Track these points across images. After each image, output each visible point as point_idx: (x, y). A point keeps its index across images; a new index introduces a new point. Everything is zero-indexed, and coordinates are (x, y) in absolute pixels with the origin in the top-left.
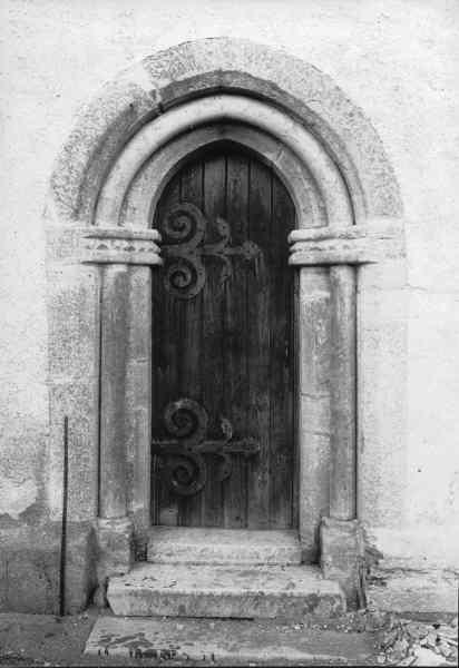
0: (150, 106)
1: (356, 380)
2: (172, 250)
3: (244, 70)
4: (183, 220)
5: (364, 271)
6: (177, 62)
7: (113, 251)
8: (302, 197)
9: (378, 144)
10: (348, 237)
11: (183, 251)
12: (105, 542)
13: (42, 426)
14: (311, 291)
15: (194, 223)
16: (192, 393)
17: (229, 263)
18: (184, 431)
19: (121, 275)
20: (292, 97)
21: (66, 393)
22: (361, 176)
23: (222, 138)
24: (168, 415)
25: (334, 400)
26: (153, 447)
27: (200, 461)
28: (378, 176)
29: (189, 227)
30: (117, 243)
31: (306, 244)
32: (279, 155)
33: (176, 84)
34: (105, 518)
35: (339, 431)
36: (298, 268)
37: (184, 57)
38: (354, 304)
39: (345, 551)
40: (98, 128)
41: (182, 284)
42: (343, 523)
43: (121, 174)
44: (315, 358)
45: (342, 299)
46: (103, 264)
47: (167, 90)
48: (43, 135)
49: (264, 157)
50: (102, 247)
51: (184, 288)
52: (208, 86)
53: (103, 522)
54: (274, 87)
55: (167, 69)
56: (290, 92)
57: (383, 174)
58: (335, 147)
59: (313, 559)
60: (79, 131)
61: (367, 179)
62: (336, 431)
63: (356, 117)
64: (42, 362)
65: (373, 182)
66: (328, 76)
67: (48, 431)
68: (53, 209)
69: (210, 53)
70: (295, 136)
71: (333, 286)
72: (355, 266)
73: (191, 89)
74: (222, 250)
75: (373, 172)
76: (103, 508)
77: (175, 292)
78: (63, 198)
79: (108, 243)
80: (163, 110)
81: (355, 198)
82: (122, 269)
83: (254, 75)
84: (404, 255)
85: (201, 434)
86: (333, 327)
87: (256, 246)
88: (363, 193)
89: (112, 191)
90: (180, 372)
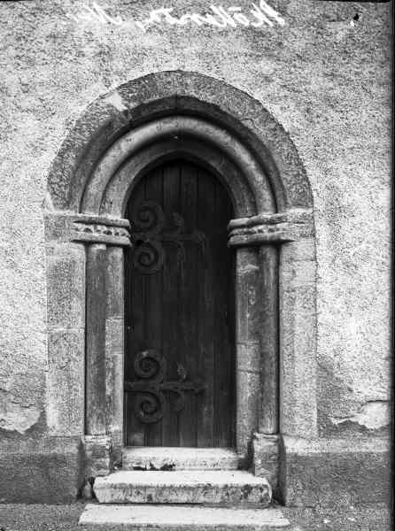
5: (286, 252)
14: (245, 266)
15: (156, 218)
18: (149, 374)
19: (101, 251)
22: (283, 176)
25: (261, 345)
27: (162, 397)
28: (295, 176)
29: (152, 219)
30: (99, 227)
34: (91, 435)
35: (267, 369)
44: (248, 315)
46: (88, 244)
47: (137, 110)
52: (168, 108)
53: (89, 438)
54: (217, 108)
56: (229, 113)
57: (298, 174)
69: (169, 83)
71: (260, 260)
75: (291, 173)
79: (91, 227)
81: (278, 193)
85: (162, 376)
89: (95, 189)
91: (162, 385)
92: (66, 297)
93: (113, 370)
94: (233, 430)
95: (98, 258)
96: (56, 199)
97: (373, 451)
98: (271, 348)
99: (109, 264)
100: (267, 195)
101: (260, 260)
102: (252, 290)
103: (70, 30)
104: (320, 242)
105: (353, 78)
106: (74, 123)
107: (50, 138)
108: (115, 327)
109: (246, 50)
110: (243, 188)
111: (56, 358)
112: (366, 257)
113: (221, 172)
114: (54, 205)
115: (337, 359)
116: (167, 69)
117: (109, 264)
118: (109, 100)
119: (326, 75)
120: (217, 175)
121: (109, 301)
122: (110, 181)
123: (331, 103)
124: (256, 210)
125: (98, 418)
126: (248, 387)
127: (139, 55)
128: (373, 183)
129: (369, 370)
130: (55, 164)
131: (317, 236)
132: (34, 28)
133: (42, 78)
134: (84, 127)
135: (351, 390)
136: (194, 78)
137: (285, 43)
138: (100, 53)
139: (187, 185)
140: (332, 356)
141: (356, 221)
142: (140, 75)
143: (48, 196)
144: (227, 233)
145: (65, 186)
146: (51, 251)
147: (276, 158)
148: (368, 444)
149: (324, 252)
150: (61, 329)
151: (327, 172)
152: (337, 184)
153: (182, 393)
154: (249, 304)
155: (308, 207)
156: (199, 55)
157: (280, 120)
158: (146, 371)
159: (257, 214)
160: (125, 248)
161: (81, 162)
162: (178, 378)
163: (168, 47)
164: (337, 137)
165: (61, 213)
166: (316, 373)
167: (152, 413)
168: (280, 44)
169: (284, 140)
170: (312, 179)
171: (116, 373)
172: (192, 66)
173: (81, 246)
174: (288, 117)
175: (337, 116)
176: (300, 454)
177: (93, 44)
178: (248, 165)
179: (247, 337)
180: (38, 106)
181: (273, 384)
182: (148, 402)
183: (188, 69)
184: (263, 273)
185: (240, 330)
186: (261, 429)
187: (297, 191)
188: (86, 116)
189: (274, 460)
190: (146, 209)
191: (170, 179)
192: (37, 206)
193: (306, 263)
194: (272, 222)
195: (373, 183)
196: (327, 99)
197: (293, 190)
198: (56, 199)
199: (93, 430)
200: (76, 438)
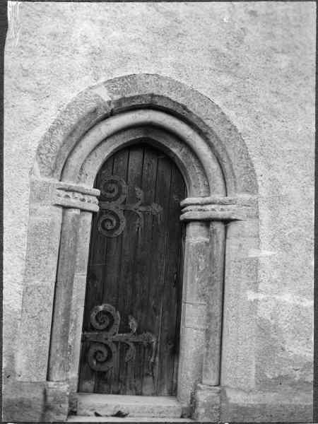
0: (106, 110)
1: (223, 293)
2: (106, 205)
3: (166, 94)
4: (114, 186)
5: (233, 228)
6: (126, 86)
7: (74, 200)
8: (193, 178)
9: (245, 149)
10: (222, 203)
11: (112, 206)
12: (52, 398)
13: (16, 313)
14: (195, 236)
15: (120, 188)
16: (111, 300)
17: (141, 216)
18: (102, 327)
19: (76, 215)
20: (195, 115)
21: (36, 292)
22: (234, 167)
23: (145, 136)
24: (93, 315)
25: (209, 306)
26: (83, 336)
27: (114, 349)
28: (244, 168)
29: (116, 192)
30: (77, 195)
31: (195, 207)
32: (181, 150)
33: (124, 99)
34: (52, 381)
35: (213, 327)
36: (187, 222)
37: (131, 83)
38: (225, 246)
39: (213, 406)
40: (72, 120)
41: (110, 228)
42: (213, 387)
43: (82, 151)
44: (197, 279)
45: (217, 242)
46: (65, 208)
47: (119, 102)
48: (34, 120)
49: (171, 151)
50: (67, 196)
51: (111, 230)
52: (144, 102)
53: (51, 384)
54: (185, 108)
55: (119, 89)
56: (194, 112)
57: (248, 167)
58: (219, 148)
59: (189, 415)
60: (59, 120)
61: (238, 170)
62: (210, 326)
63: (233, 132)
64: (20, 268)
65: (241, 171)
66: (217, 106)
67: (20, 316)
68: (37, 169)
69: (148, 83)
70: (193, 139)
71: (211, 234)
72: (226, 222)
73: (133, 104)
74: (137, 207)
75: (241, 165)
76: (50, 375)
77: (105, 233)
78: (45, 162)
79: (70, 194)
80: (112, 114)
81: (228, 181)
82: (77, 212)
83: (173, 99)
84: (258, 217)
85: (115, 328)
86: (211, 258)
87: (160, 207)
88: (235, 177)
89: (75, 162)
90: (103, 284)
91: (114, 337)
92: (44, 254)
93: (76, 321)
94: (175, 381)
95: (73, 221)
96: (43, 167)
97: (301, 403)
98: (216, 310)
99: (81, 226)
100: (219, 181)
101: (211, 234)
102: (201, 258)
103: (67, 33)
104: (263, 223)
105: (292, 97)
106: (65, 106)
107: (42, 115)
108: (81, 278)
109: (210, 66)
110: (199, 173)
111: (29, 308)
112: (298, 237)
113: (181, 158)
114: (41, 172)
115: (273, 322)
116: (146, 72)
117: (81, 226)
118: (96, 91)
119: (272, 92)
120: (176, 161)
121: (78, 260)
122: (88, 157)
123: (275, 114)
124: (209, 192)
125: (61, 365)
126: (194, 342)
127: (125, 59)
128: (305, 179)
129: (298, 333)
130: (45, 138)
131: (260, 218)
132: (38, 27)
133: (40, 66)
134: (74, 110)
135: (283, 349)
136: (168, 82)
137: (241, 64)
138: (92, 53)
139: (149, 165)
140: (269, 319)
141: (292, 208)
142: (124, 74)
143: (36, 165)
144: (180, 210)
145: (52, 159)
146: (32, 212)
147: (230, 152)
148: (296, 398)
149: (265, 231)
150: (37, 282)
151: (270, 167)
152: (278, 177)
153: (131, 345)
154: (198, 269)
155: (253, 193)
156: (174, 65)
157: (235, 123)
158: (101, 324)
159: (209, 196)
160: (94, 213)
161: (67, 138)
162: (129, 331)
163: (148, 56)
164: (279, 140)
165: (47, 180)
166: (256, 333)
167: (102, 363)
168: (237, 64)
169: (238, 139)
170: (258, 172)
171: (77, 325)
172: (167, 72)
173: (60, 210)
174: (241, 122)
175: (279, 124)
176: (240, 405)
177: (87, 45)
178: (206, 155)
179: (195, 298)
180: (35, 89)
181: (217, 340)
182: (101, 352)
183: (163, 74)
184: (213, 243)
185: (188, 292)
186: (204, 381)
187: (245, 181)
188: (75, 102)
189: (216, 409)
190: (112, 182)
191: (135, 159)
192: (26, 172)
193: (250, 239)
194: (222, 203)
195: (305, 179)
196: (272, 111)
197: (243, 179)
198: (43, 167)
199: (56, 376)
200: (41, 384)
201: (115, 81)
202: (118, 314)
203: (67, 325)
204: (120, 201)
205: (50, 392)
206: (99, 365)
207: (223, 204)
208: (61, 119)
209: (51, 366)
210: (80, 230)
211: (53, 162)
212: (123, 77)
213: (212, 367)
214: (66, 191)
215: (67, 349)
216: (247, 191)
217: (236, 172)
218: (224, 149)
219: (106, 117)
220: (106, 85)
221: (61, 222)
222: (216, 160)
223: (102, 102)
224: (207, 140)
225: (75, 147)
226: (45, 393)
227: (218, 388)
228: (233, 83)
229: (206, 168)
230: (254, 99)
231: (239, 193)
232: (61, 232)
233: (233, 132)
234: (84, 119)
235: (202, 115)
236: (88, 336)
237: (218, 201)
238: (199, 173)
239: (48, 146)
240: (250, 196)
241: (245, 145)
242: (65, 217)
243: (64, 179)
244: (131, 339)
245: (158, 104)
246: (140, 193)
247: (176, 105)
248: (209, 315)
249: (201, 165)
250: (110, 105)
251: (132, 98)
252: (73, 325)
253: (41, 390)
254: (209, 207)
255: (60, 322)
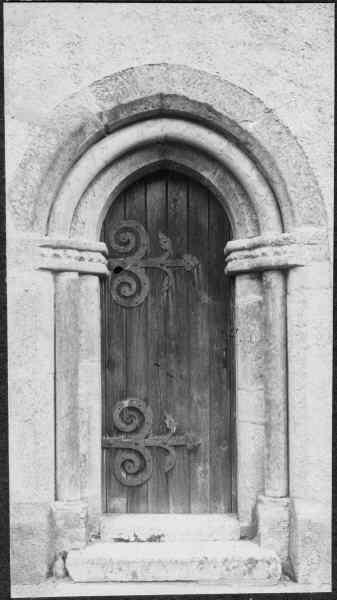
4: (129, 236)
5: (293, 275)
7: (67, 260)
10: (278, 244)
14: (245, 294)
15: (138, 242)
17: (171, 274)
18: (131, 428)
19: (72, 281)
23: (162, 158)
25: (267, 391)
27: (147, 454)
29: (133, 241)
30: (69, 252)
31: (240, 253)
32: (214, 173)
33: (121, 107)
36: (233, 276)
38: (285, 305)
39: (279, 524)
46: (56, 272)
47: (114, 112)
50: (56, 256)
52: (151, 109)
54: (210, 109)
56: (225, 113)
66: (259, 99)
71: (265, 289)
72: (284, 271)
73: (135, 112)
77: (121, 301)
78: (19, 211)
79: (60, 252)
80: (108, 131)
81: (284, 209)
82: (75, 275)
85: (146, 429)
87: (195, 258)
89: (64, 207)
98: (278, 396)
101: (265, 289)
110: (243, 204)
124: (258, 230)
125: (71, 481)
137: (291, 29)
144: (222, 258)
159: (259, 235)
165: (24, 235)
167: (136, 474)
173: (49, 276)
182: (131, 461)
183: (174, 60)
186: (267, 492)
194: (278, 244)
199: (65, 493)
201: (105, 82)
202: (149, 410)
203: (75, 427)
204: (138, 256)
205: (58, 515)
206: (129, 478)
207: (277, 245)
208: (35, 148)
209: (59, 482)
210: (83, 300)
211: (31, 210)
212: (116, 74)
213: (278, 473)
214: (55, 248)
215: (81, 460)
216: (311, 223)
217: (292, 196)
218: (273, 164)
219: (100, 137)
220: (94, 88)
221: (53, 292)
222: (264, 182)
223: (90, 116)
224: (248, 154)
225: (61, 186)
226: (51, 515)
227: (286, 500)
228: (281, 61)
229: (251, 195)
230: (314, 82)
231: (300, 226)
232: (55, 306)
233: (284, 136)
234: (67, 143)
235: (238, 117)
236: (111, 442)
237: (270, 241)
238: (243, 204)
239: (21, 188)
240: (317, 230)
241: (304, 153)
242: (58, 284)
243: (51, 234)
244: (170, 442)
245: (172, 108)
246: (166, 242)
247: (197, 106)
248: (268, 403)
249: (245, 192)
250: (101, 117)
251: (132, 104)
252: (85, 428)
253: (45, 513)
254: (258, 252)
255: (64, 425)
